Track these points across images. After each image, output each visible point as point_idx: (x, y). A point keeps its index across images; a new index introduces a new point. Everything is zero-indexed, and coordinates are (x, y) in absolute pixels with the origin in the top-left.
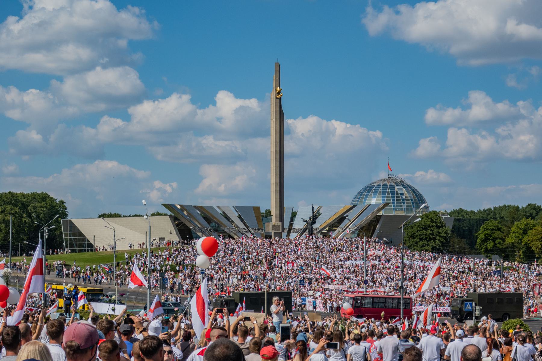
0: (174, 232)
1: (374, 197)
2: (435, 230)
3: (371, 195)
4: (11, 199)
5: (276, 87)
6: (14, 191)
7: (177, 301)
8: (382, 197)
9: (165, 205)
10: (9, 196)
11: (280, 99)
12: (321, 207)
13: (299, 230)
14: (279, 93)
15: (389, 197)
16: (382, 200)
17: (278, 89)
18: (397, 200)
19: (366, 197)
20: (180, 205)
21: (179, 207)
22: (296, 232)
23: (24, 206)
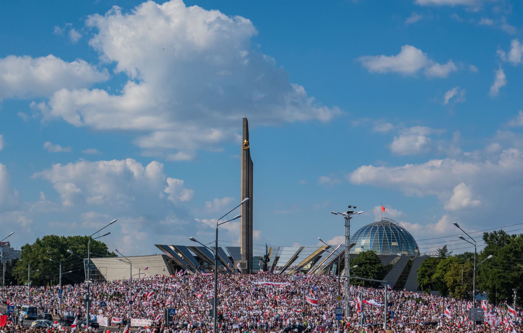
0: (166, 269)
1: (363, 239)
2: (368, 266)
3: (362, 236)
4: (52, 242)
5: (244, 140)
6: (55, 234)
7: (73, 315)
8: (371, 238)
9: (157, 246)
10: (50, 239)
11: (248, 150)
12: (303, 247)
13: (281, 267)
14: (246, 145)
15: (386, 238)
16: (371, 241)
17: (245, 141)
18: (384, 241)
19: (357, 239)
20: (173, 246)
21: (172, 248)
22: (279, 270)
23: (62, 250)
